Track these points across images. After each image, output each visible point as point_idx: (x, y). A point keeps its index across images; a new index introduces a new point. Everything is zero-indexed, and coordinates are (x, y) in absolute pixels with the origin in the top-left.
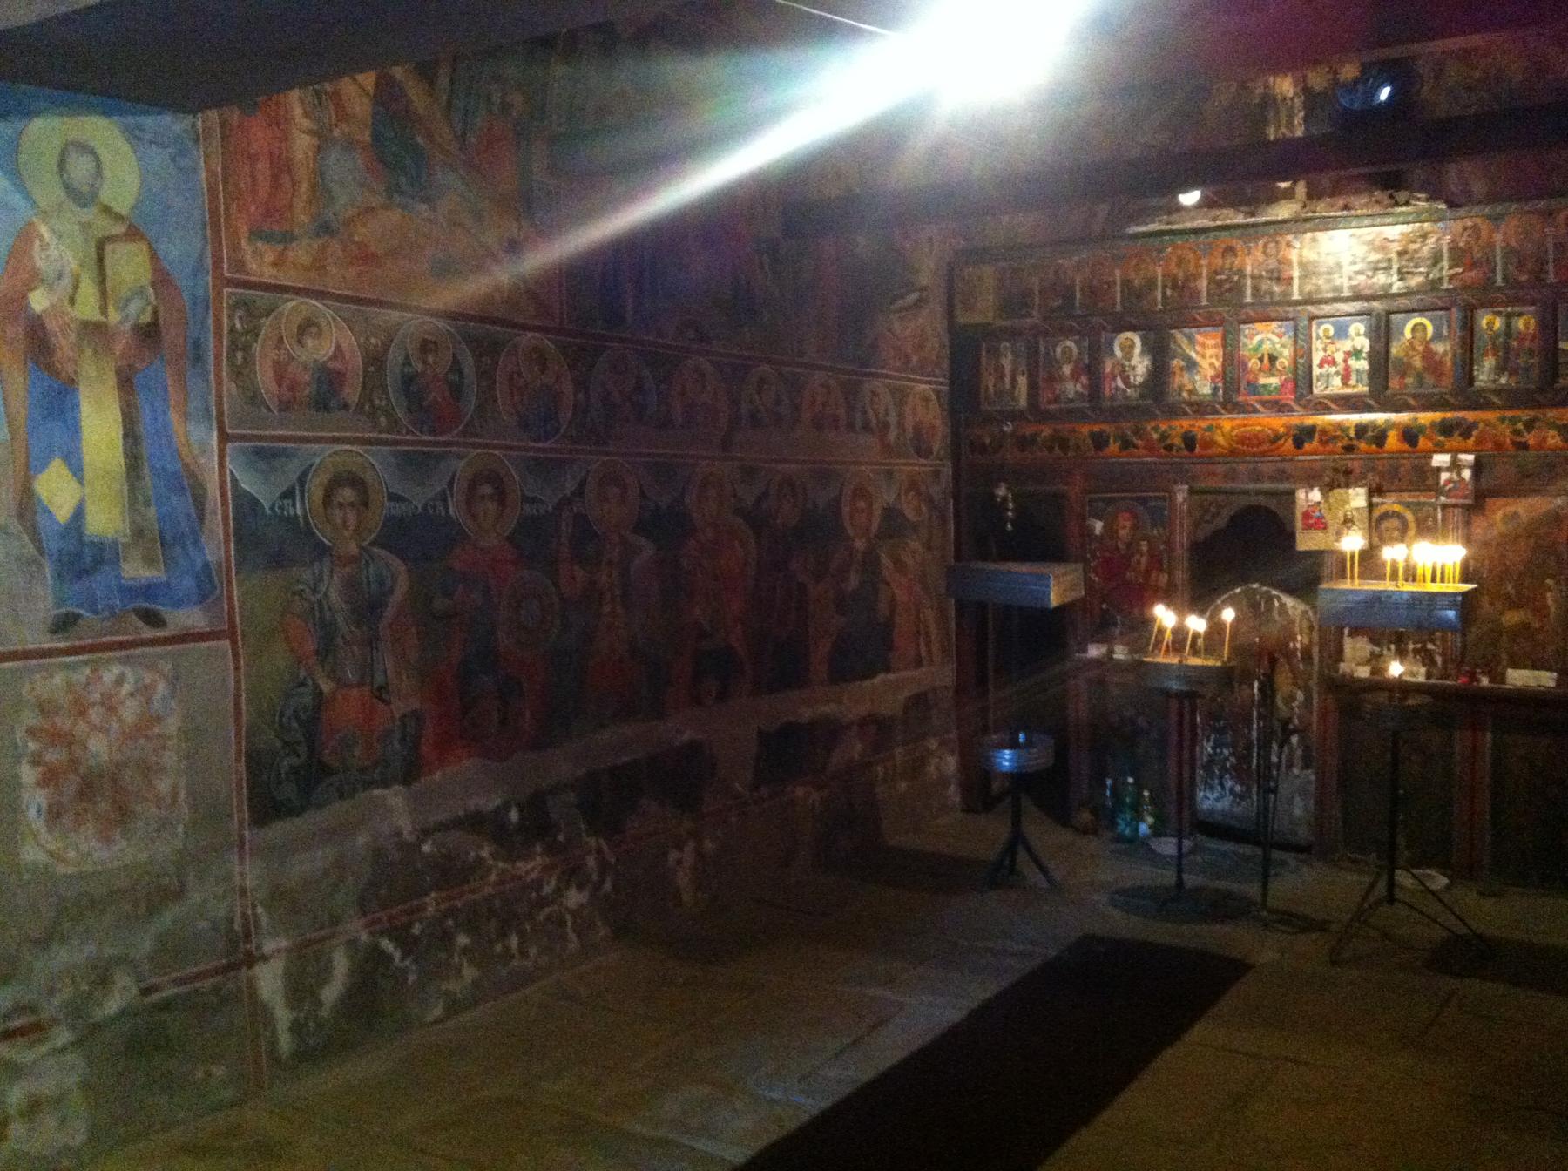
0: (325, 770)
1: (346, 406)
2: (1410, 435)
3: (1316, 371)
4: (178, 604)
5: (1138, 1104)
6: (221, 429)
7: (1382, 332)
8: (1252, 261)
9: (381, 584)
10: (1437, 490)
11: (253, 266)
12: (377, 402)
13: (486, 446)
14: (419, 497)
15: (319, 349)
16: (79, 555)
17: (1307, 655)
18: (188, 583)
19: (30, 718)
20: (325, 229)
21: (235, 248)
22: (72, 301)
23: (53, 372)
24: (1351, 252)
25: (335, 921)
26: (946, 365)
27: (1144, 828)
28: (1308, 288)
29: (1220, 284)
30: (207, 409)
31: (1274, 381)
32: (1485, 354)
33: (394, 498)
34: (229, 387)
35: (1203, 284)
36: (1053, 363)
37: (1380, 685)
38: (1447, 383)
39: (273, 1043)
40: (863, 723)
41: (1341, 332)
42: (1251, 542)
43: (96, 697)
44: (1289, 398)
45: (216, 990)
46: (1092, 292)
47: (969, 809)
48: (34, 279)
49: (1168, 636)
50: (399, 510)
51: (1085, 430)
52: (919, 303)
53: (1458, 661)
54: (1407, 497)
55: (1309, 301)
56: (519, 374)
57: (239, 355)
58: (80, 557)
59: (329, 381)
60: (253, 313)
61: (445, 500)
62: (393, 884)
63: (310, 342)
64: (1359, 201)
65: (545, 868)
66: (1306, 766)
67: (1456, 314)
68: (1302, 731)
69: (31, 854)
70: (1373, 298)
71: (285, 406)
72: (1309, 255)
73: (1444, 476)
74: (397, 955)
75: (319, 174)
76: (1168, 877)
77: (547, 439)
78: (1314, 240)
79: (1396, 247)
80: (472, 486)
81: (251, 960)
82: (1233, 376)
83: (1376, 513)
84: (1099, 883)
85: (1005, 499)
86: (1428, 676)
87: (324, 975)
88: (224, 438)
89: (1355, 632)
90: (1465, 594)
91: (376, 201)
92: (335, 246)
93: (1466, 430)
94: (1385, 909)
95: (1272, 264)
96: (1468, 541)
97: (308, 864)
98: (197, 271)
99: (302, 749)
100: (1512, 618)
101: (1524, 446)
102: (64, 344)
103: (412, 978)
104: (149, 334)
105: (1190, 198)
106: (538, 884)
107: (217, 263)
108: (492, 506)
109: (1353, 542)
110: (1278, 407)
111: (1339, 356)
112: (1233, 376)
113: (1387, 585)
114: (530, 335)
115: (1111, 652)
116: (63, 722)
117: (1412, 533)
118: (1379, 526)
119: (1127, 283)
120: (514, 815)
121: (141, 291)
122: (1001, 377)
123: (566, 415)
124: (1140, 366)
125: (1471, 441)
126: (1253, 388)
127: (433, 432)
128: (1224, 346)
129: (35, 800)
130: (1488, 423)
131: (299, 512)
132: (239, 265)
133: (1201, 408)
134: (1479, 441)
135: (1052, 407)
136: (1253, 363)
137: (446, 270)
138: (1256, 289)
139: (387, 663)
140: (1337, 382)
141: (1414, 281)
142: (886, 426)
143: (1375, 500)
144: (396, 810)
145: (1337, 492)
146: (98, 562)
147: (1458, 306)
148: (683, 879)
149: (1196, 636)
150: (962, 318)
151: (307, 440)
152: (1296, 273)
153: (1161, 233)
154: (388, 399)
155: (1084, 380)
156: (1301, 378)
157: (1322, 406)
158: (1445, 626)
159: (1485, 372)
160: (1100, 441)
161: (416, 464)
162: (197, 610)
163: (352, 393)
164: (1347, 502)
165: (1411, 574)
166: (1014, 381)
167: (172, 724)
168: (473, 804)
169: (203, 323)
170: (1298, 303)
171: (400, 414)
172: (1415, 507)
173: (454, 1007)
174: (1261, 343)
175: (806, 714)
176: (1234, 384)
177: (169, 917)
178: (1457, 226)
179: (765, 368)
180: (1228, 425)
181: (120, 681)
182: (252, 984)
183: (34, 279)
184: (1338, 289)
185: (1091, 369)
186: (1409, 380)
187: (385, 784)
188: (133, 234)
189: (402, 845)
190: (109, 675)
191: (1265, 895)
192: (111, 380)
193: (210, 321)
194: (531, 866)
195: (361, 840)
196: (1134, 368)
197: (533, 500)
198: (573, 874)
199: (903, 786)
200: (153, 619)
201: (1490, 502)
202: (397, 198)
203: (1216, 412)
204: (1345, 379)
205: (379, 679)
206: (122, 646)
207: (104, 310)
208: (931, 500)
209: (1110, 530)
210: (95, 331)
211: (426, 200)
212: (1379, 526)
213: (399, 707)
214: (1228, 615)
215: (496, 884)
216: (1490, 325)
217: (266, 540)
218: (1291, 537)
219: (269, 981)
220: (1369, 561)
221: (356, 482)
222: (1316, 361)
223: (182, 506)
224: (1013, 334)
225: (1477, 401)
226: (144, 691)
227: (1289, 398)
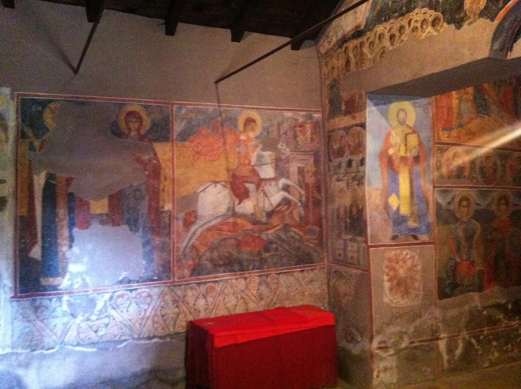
18: (424, 228)
45: (428, 346)
50: (479, 208)
92: (463, 131)
98: (429, 140)
120: (510, 306)
132: (439, 138)
144: (476, 300)
161: (483, 194)
167: (419, 268)
168: (499, 301)
177: (418, 322)
181: (407, 254)
187: (473, 291)
188: (414, 132)
200: (415, 237)
202: (480, 114)
205: (472, 259)
213: (478, 268)
221: (467, 199)
223: (423, 206)
226: (412, 257)
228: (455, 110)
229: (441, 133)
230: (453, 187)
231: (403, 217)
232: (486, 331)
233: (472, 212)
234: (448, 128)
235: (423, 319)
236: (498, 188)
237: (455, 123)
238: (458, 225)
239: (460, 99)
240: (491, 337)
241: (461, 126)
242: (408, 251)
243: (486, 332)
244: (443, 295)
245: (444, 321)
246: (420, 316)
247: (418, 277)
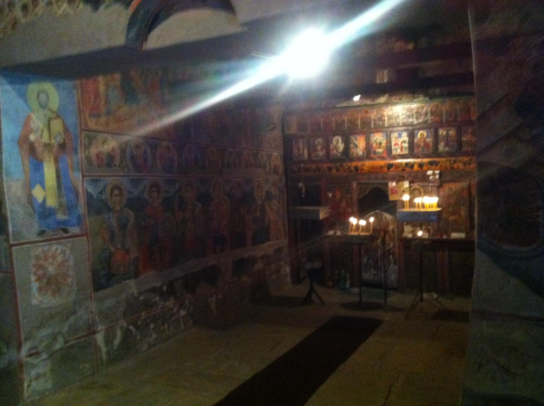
0: (113, 275)
1: (115, 166)
2: (421, 165)
3: (393, 147)
4: (73, 225)
5: (355, 359)
6: (83, 174)
7: (412, 136)
8: (373, 115)
10: (429, 182)
14: (136, 192)
16: (44, 212)
17: (393, 231)
18: (74, 220)
19: (33, 262)
20: (108, 113)
21: (85, 119)
22: (41, 137)
23: (36, 158)
24: (401, 111)
25: (117, 320)
26: (282, 146)
27: (348, 286)
28: (390, 123)
29: (364, 122)
31: (381, 150)
32: (441, 142)
33: (130, 192)
35: (359, 122)
36: (315, 147)
37: (415, 238)
38: (431, 150)
39: (101, 358)
40: (263, 257)
41: (400, 136)
42: (376, 198)
43: (50, 254)
44: (385, 155)
45: (85, 341)
46: (326, 124)
47: (294, 283)
48: (31, 131)
49: (354, 228)
50: (131, 196)
51: (325, 166)
52: (274, 128)
53: (438, 230)
54: (421, 184)
55: (390, 126)
58: (45, 213)
59: (111, 157)
62: (133, 308)
64: (404, 97)
65: (174, 304)
66: (395, 264)
67: (432, 130)
68: (393, 254)
69: (35, 302)
70: (408, 125)
71: (99, 166)
72: (390, 113)
73: (431, 178)
74: (134, 330)
75: (107, 96)
76: (357, 299)
78: (391, 109)
79: (415, 111)
80: (151, 187)
81: (95, 332)
82: (369, 148)
83: (412, 188)
84: (334, 301)
85: (302, 188)
86: (429, 236)
87: (114, 337)
88: (83, 176)
89: (407, 224)
90: (439, 212)
93: (437, 164)
94: (419, 304)
95: (379, 116)
96: (438, 196)
97: (109, 303)
100: (452, 218)
101: (453, 168)
102: (39, 150)
103: (139, 338)
104: (62, 146)
105: (357, 98)
106: (172, 309)
107: (81, 124)
108: (156, 194)
109: (406, 197)
110: (383, 158)
111: (400, 141)
112: (369, 148)
113: (416, 210)
115: (335, 233)
116: (42, 262)
117: (422, 194)
118: (413, 193)
119: (336, 122)
120: (165, 288)
121: (60, 134)
122: (299, 150)
124: (341, 146)
125: (438, 167)
126: (375, 153)
128: (366, 140)
129: (35, 286)
130: (443, 162)
132: (86, 124)
133: (360, 159)
134: (441, 167)
135: (315, 159)
136: (374, 145)
137: (141, 123)
138: (375, 124)
140: (399, 150)
141: (421, 120)
142: (265, 166)
143: (412, 185)
144: (132, 287)
145: (400, 183)
146: (50, 214)
147: (433, 127)
148: (213, 306)
149: (363, 227)
150: (287, 132)
152: (386, 119)
153: (346, 107)
155: (325, 151)
156: (389, 149)
157: (395, 158)
158: (432, 221)
159: (441, 147)
160: (330, 169)
161: (135, 182)
163: (117, 161)
164: (403, 186)
165: (423, 206)
166: (303, 152)
167: (71, 263)
169: (77, 143)
170: (387, 127)
171: (131, 167)
172: (423, 187)
173: (150, 346)
174: (377, 139)
175: (246, 255)
176: (369, 151)
177: (72, 320)
178: (432, 105)
179: (231, 150)
180: (368, 163)
181: (57, 250)
182: (95, 339)
183: (31, 131)
184: (398, 123)
185: (327, 147)
186: (420, 149)
187: (129, 278)
188: (58, 116)
190: (54, 248)
191: (386, 303)
192: (52, 160)
193: (79, 141)
194: (170, 303)
195: (123, 296)
196: (339, 148)
197: (167, 192)
198: (182, 305)
199: (274, 277)
200: (65, 231)
201: (444, 184)
203: (364, 160)
204: (402, 149)
206: (55, 239)
207: (50, 139)
208: (279, 188)
209: (334, 196)
210: (47, 146)
212: (413, 193)
214: (372, 220)
216: (442, 133)
217: (96, 206)
218: (387, 197)
219: (100, 338)
220: (411, 203)
222: (393, 144)
224: (303, 137)
225: (440, 155)
226: (64, 252)
227: (385, 155)
237: (103, 110)
243: (143, 317)
246: (75, 313)
247: (71, 273)
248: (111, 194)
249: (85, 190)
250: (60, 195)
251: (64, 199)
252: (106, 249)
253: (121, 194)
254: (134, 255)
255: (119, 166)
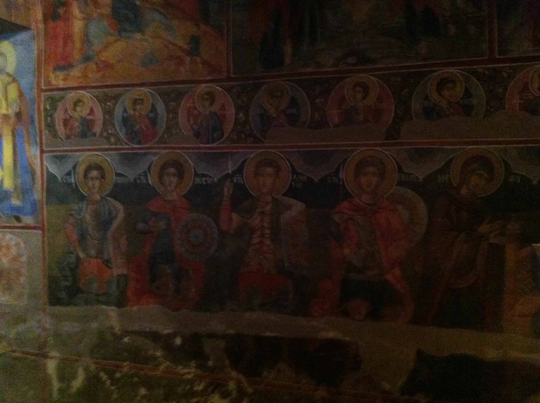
0: (79, 291)
1: (94, 135)
9: (110, 213)
11: (54, 82)
12: (110, 131)
13: (172, 148)
14: (131, 175)
15: (82, 112)
18: (28, 206)
21: (47, 77)
30: (36, 142)
33: (118, 175)
34: (45, 132)
45: (34, 361)
50: (120, 180)
56: (195, 108)
57: (49, 119)
60: (53, 102)
61: (146, 176)
62: (107, 348)
63: (78, 109)
71: (68, 137)
74: (108, 382)
77: (213, 143)
80: (163, 168)
87: (74, 376)
88: (42, 152)
91: (112, 39)
92: (92, 66)
97: (68, 327)
98: (31, 89)
99: (70, 279)
103: (115, 396)
104: (18, 115)
107: (38, 84)
108: (174, 180)
114: (203, 85)
120: (178, 341)
123: (229, 127)
127: (139, 143)
131: (73, 181)
132: (49, 83)
139: (110, 249)
144: (112, 317)
151: (71, 151)
154: (116, 130)
161: (129, 159)
162: (30, 218)
167: (24, 259)
168: (155, 327)
171: (122, 136)
175: (491, 354)
177: (21, 328)
181: (11, 240)
187: (107, 303)
188: (14, 80)
189: (114, 335)
192: (10, 133)
200: (18, 219)
202: (124, 34)
205: (106, 257)
211: (140, 31)
213: (117, 271)
215: (163, 372)
217: (60, 192)
221: (99, 168)
223: (28, 178)
226: (17, 244)
228: (77, 39)
229: (52, 76)
230: (71, 151)
231: (6, 192)
232: (126, 366)
233: (108, 189)
234: (65, 65)
235: (28, 325)
236: (160, 148)
237: (77, 56)
238: (83, 205)
239: (87, 19)
240: (136, 379)
241: (87, 59)
242: (11, 236)
243: (126, 369)
244: (55, 300)
245: (57, 335)
246: (24, 321)
247: (23, 271)
248: (86, 176)
249: (45, 171)
250: (15, 176)
251: (19, 181)
252: (71, 253)
253: (103, 177)
254: (119, 269)
255: (101, 135)
